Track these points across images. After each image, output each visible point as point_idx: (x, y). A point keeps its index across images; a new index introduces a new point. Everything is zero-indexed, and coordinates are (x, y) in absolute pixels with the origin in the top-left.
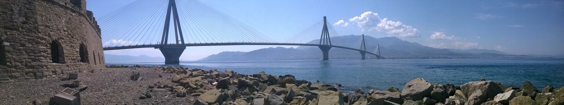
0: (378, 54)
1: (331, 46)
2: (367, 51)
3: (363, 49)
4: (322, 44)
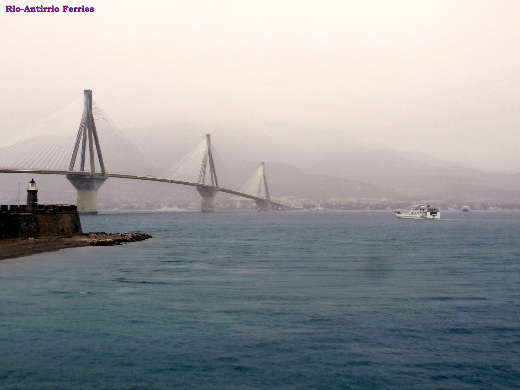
0: (263, 196)
1: (103, 177)
2: (220, 186)
3: (208, 182)
4: (77, 169)
